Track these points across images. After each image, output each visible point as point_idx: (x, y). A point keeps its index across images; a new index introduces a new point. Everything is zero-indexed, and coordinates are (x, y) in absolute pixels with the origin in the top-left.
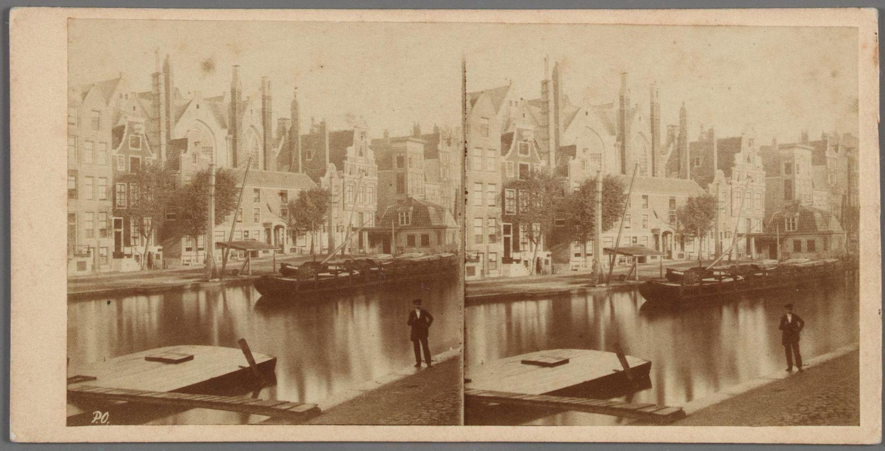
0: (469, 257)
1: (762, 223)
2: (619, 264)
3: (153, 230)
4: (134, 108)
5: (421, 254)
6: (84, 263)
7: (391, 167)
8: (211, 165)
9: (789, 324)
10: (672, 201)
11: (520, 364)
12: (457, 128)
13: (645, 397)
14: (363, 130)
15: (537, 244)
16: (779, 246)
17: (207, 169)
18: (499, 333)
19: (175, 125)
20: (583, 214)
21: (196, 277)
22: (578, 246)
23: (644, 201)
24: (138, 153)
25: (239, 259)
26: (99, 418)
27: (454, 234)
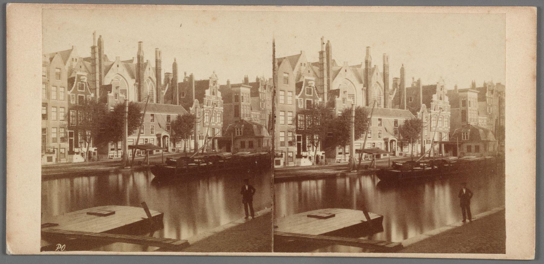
0: (277, 154)
1: (448, 135)
2: (364, 159)
3: (319, 142)
4: (81, 67)
5: (249, 153)
6: (51, 157)
7: (458, 107)
8: (126, 100)
9: (247, 191)
10: (396, 122)
11: (86, 214)
12: (270, 79)
13: (379, 236)
14: (214, 80)
15: (316, 147)
16: (458, 148)
17: (123, 102)
18: (294, 198)
19: (333, 81)
20: (344, 129)
21: (115, 166)
22: (113, 144)
23: (379, 122)
24: (311, 97)
25: (369, 159)
26: (60, 248)
27: (268, 141)
